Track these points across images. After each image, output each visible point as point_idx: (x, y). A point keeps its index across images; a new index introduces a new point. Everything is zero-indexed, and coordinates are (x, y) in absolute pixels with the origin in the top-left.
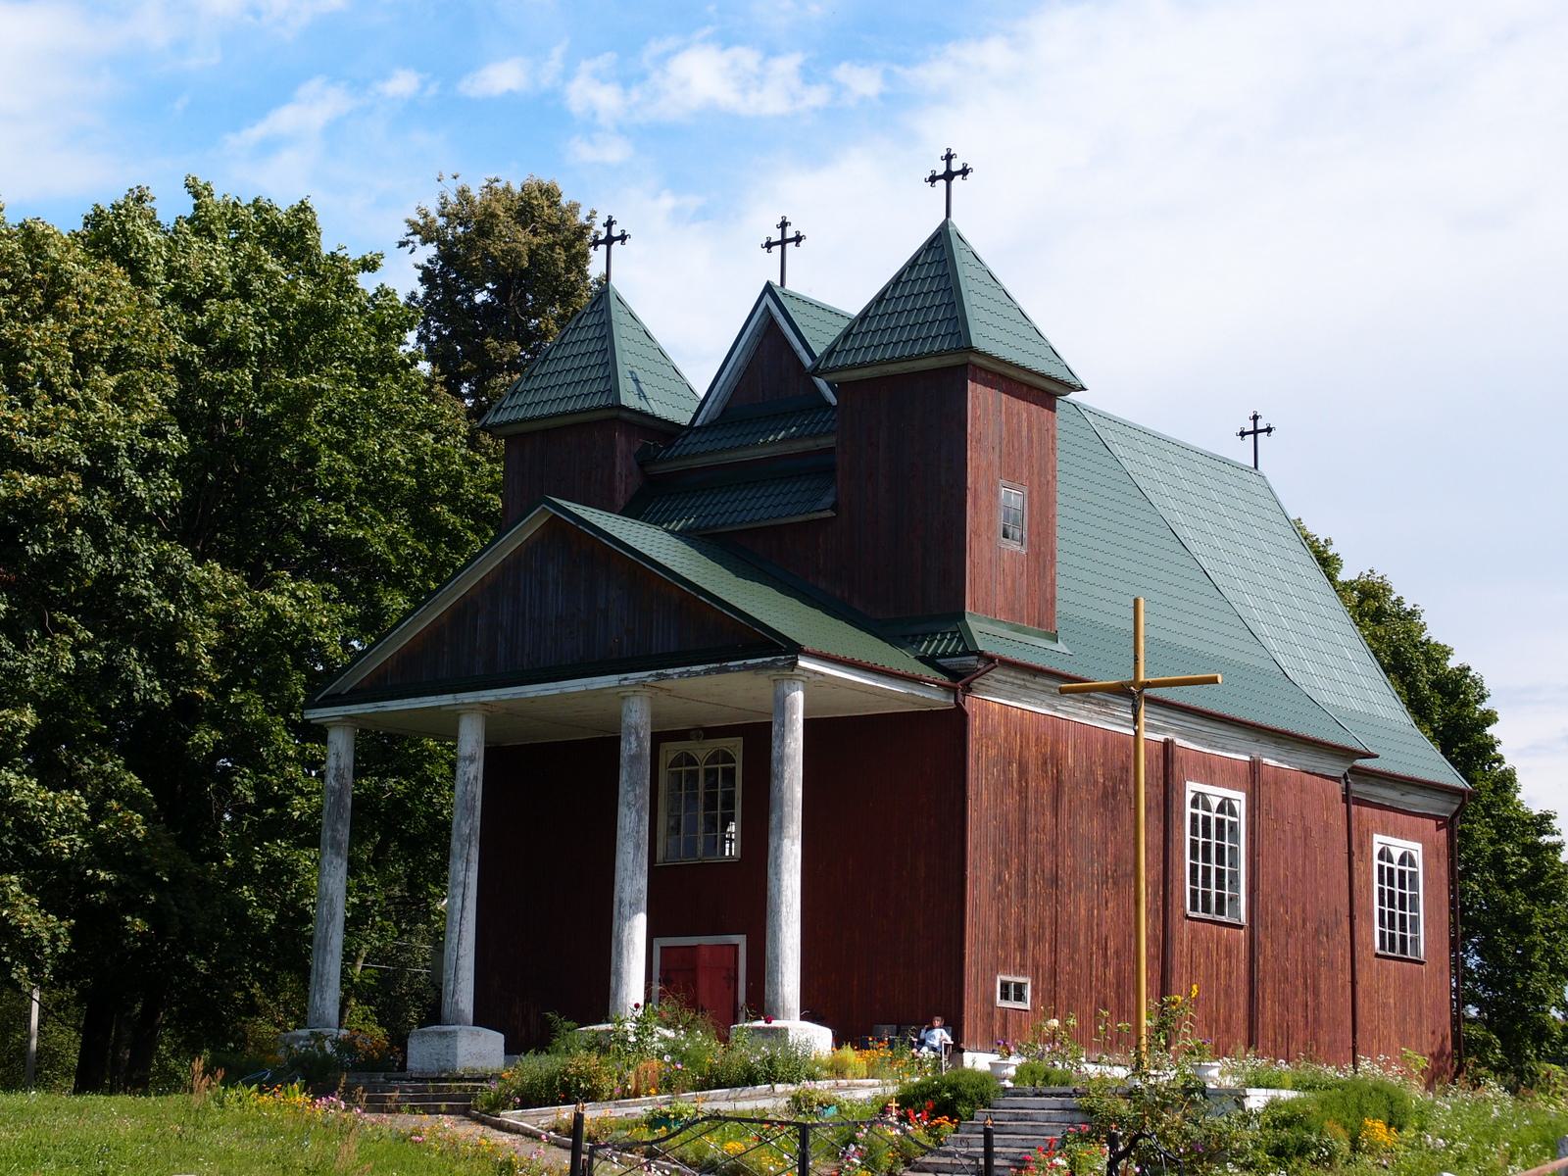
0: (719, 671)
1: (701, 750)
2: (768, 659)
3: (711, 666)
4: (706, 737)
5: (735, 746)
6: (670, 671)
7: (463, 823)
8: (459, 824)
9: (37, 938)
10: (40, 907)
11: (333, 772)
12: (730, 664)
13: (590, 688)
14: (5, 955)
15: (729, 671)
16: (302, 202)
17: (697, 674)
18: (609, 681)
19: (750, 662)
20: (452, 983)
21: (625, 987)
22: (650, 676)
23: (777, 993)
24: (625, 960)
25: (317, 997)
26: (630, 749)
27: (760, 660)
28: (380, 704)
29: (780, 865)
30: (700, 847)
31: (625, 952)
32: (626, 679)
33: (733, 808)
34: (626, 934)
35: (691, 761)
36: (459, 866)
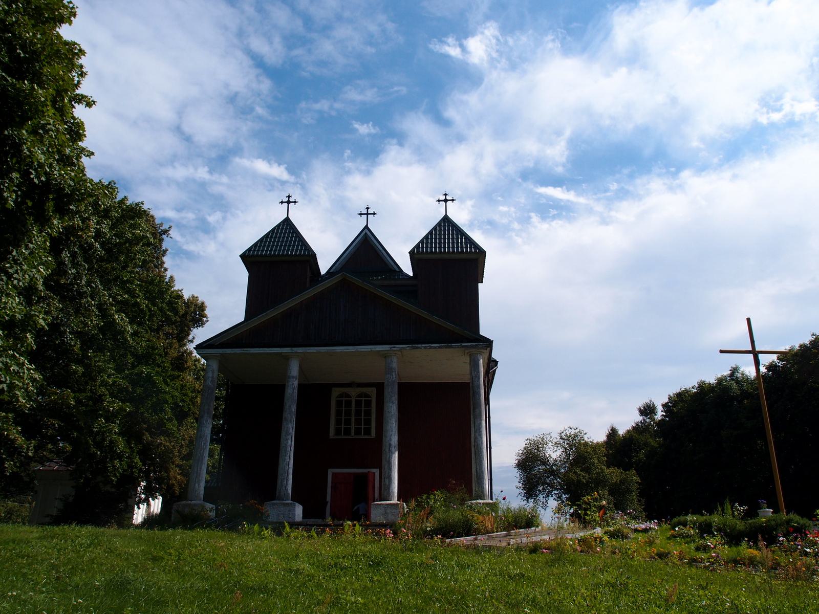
0: (446, 347)
1: (353, 392)
2: (474, 344)
3: (442, 345)
4: (357, 387)
5: (372, 392)
6: (419, 346)
7: (292, 406)
8: (290, 406)
9: (22, 447)
10: (21, 433)
11: (210, 379)
12: (453, 345)
13: (373, 350)
14: (3, 454)
15: (453, 347)
16: (100, 180)
17: (435, 348)
18: (386, 347)
19: (463, 344)
20: (285, 480)
21: (393, 484)
22: (408, 347)
23: (484, 488)
24: (393, 472)
25: (197, 485)
26: (393, 378)
27: (469, 344)
28: (245, 349)
29: (481, 432)
30: (353, 431)
31: (393, 468)
32: (394, 347)
33: (350, 425)
34: (393, 460)
35: (348, 396)
36: (290, 425)
